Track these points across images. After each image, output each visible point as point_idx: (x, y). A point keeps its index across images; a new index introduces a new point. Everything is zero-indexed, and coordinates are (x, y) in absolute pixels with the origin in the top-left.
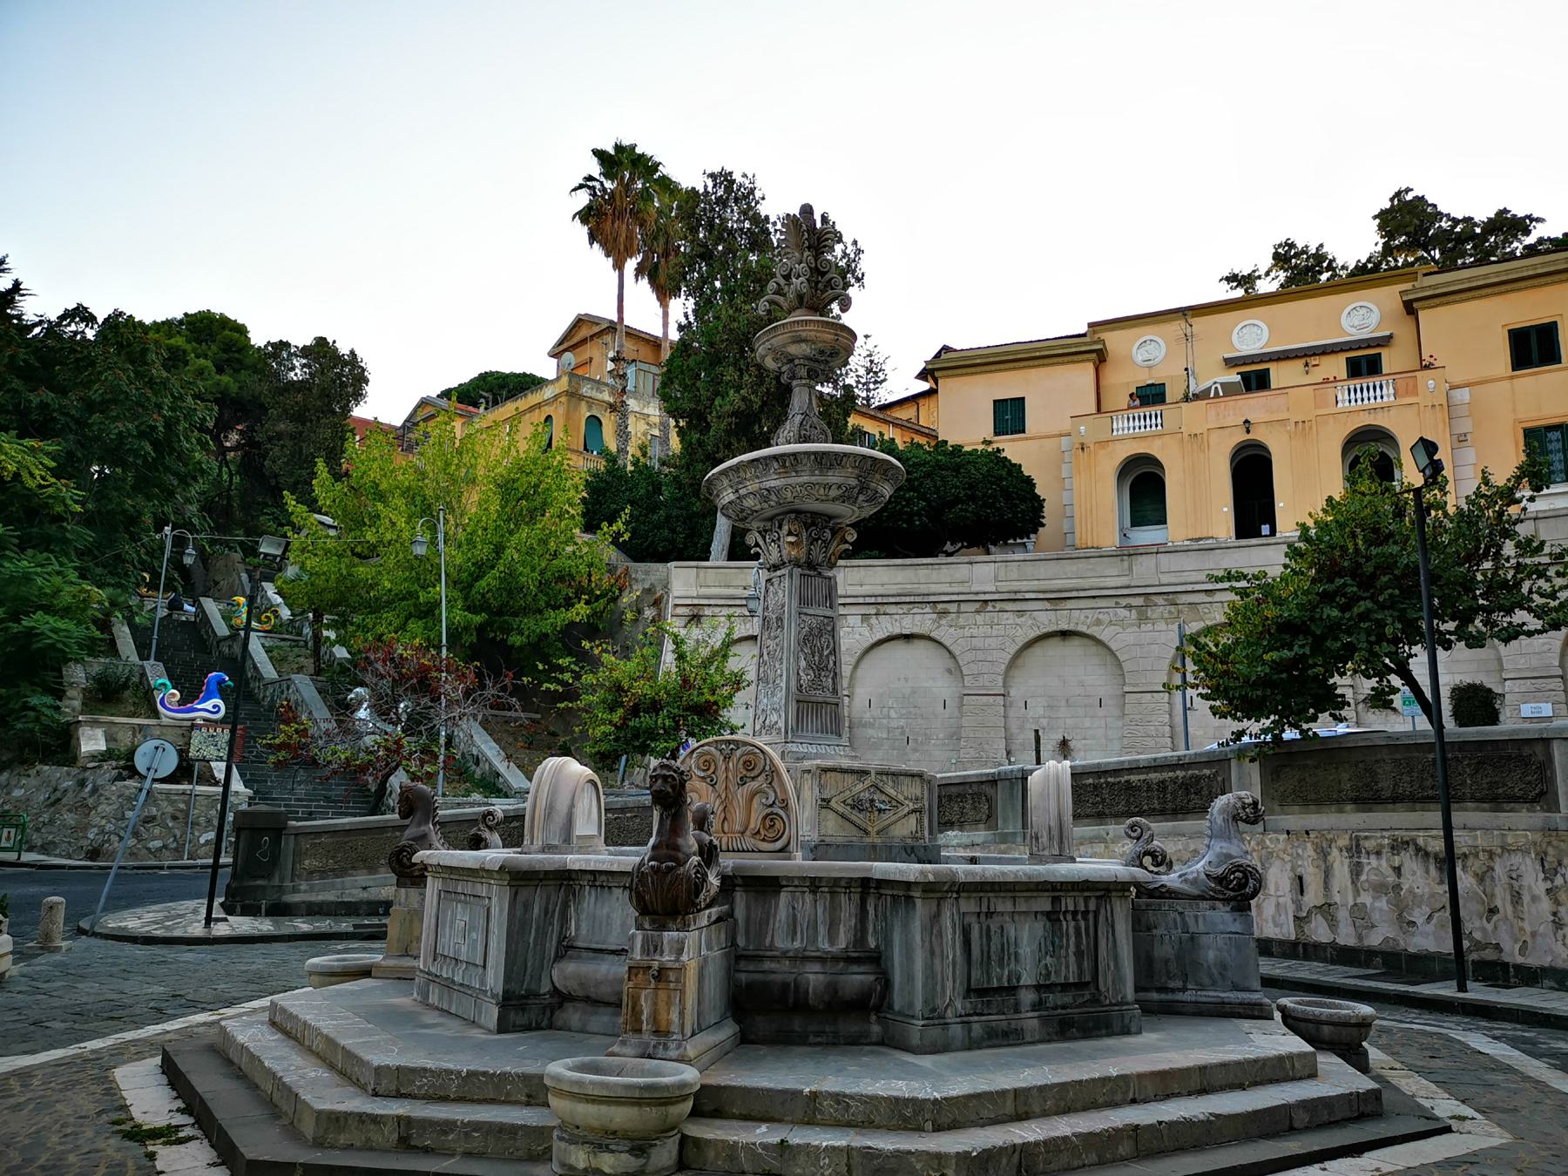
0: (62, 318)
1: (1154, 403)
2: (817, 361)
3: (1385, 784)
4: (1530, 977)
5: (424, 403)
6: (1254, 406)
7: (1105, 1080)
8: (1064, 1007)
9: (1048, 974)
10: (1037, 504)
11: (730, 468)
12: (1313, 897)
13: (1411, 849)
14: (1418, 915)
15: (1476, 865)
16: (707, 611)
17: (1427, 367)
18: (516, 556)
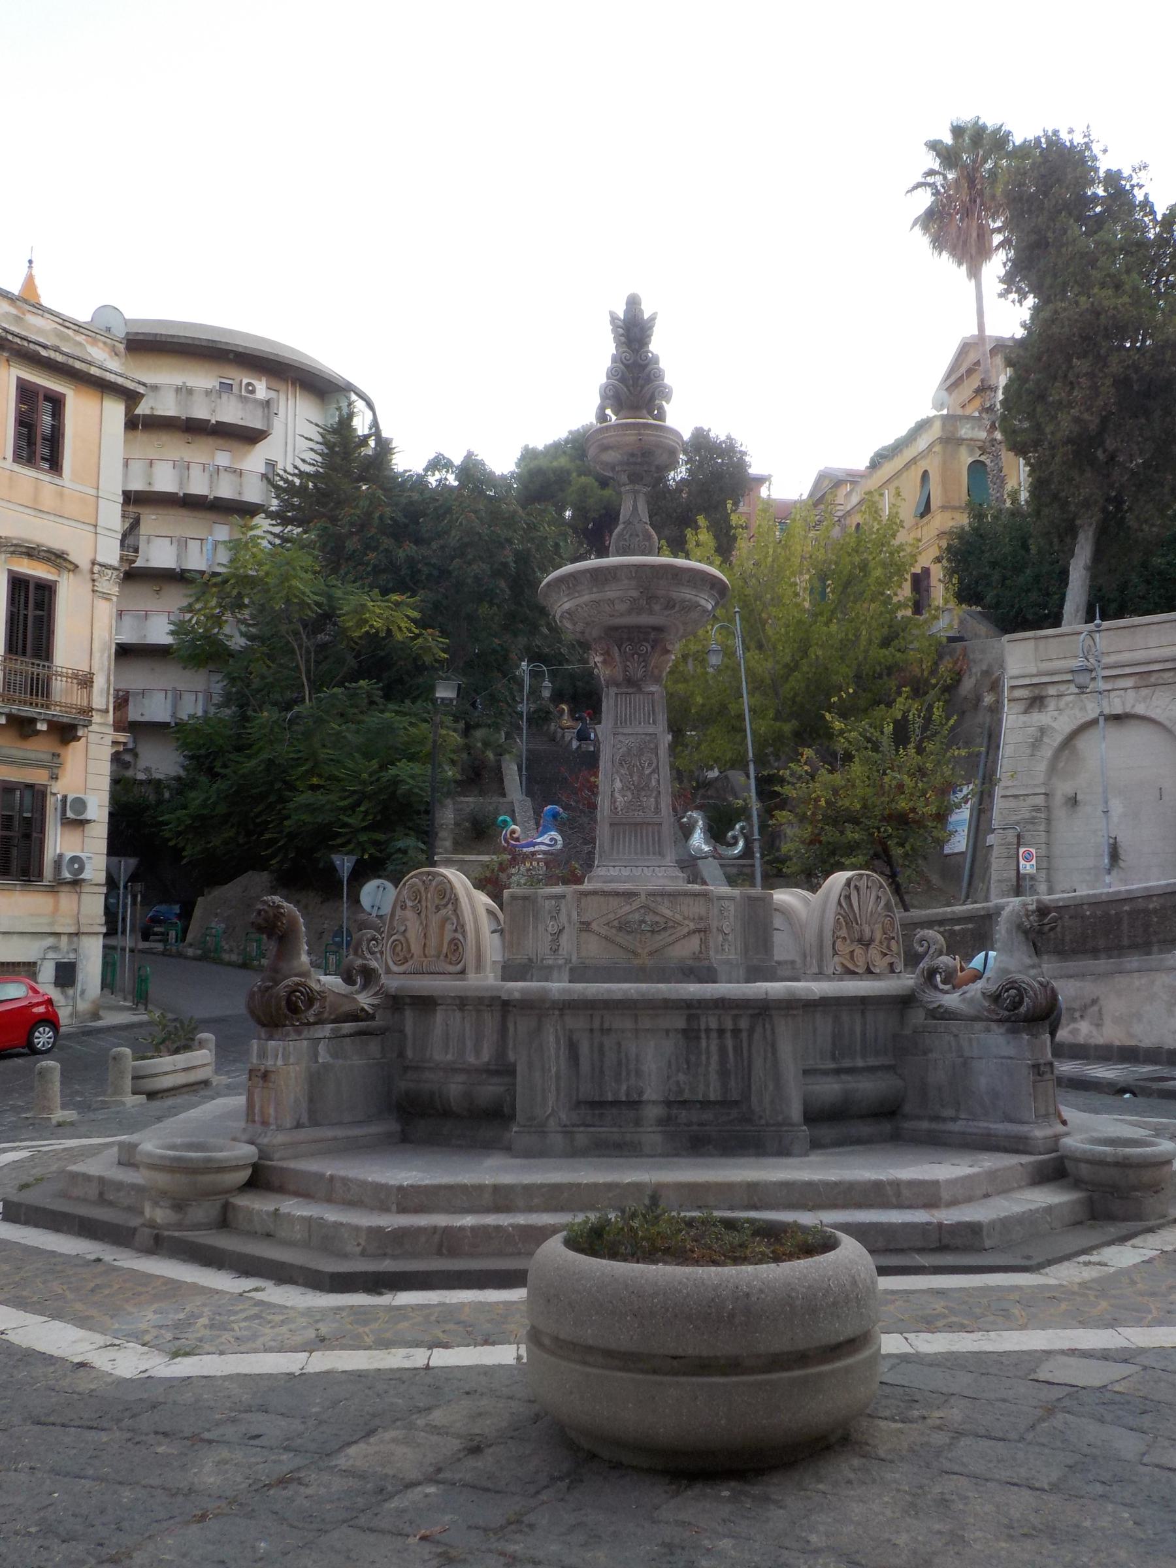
0: (426, 470)
9: (681, 1092)
16: (1052, 691)
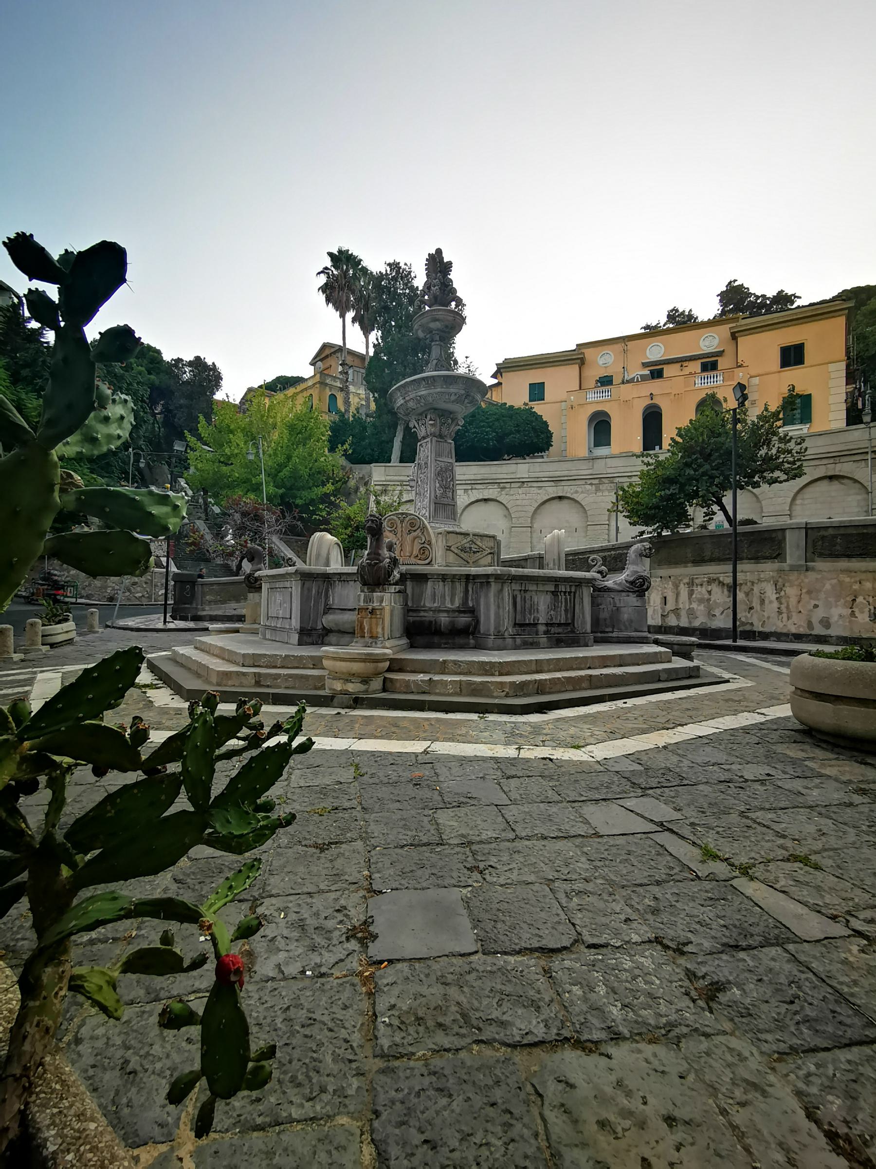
1: (607, 385)
2: (444, 332)
3: (707, 554)
4: (765, 636)
5: (250, 390)
6: (655, 386)
7: (577, 658)
9: (552, 619)
10: (549, 435)
12: (670, 606)
13: (717, 582)
14: (717, 612)
15: (745, 588)
17: (740, 366)
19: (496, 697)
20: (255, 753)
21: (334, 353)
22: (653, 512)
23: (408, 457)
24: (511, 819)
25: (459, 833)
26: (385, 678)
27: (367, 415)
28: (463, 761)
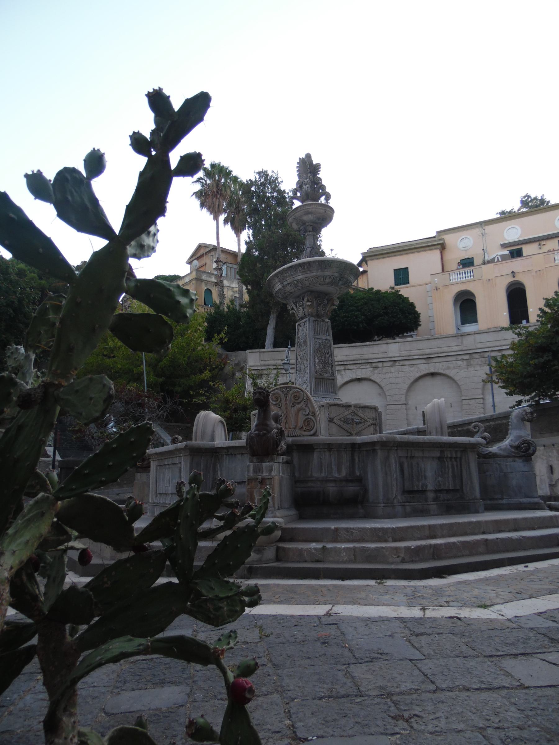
2: (317, 223)
6: (516, 264)
7: (470, 523)
8: (448, 500)
11: (279, 272)
16: (265, 372)
18: (176, 350)
19: (392, 563)
20: (228, 533)
21: (209, 251)
22: (529, 380)
23: (286, 339)
24: (429, 672)
25: (377, 685)
26: (278, 549)
27: (242, 306)
28: (368, 621)
